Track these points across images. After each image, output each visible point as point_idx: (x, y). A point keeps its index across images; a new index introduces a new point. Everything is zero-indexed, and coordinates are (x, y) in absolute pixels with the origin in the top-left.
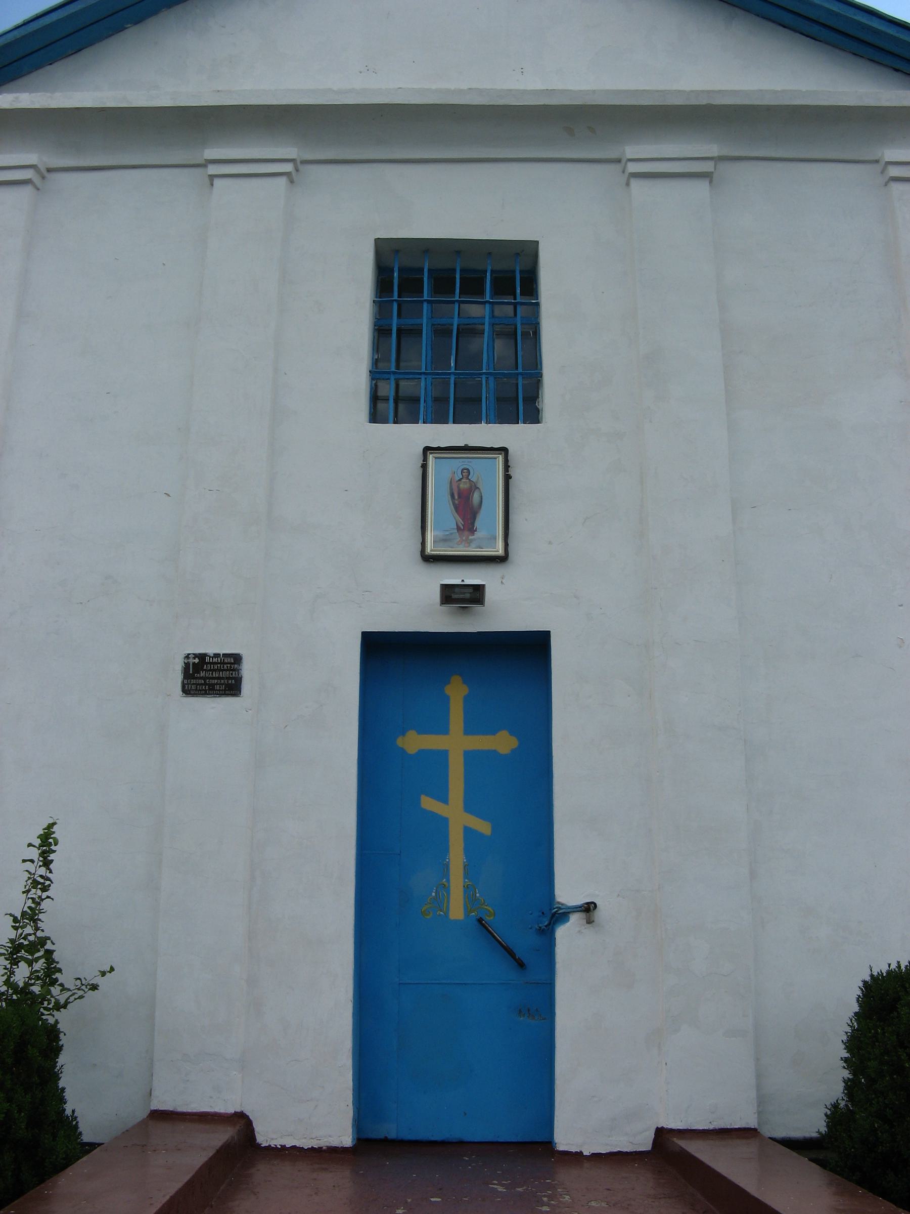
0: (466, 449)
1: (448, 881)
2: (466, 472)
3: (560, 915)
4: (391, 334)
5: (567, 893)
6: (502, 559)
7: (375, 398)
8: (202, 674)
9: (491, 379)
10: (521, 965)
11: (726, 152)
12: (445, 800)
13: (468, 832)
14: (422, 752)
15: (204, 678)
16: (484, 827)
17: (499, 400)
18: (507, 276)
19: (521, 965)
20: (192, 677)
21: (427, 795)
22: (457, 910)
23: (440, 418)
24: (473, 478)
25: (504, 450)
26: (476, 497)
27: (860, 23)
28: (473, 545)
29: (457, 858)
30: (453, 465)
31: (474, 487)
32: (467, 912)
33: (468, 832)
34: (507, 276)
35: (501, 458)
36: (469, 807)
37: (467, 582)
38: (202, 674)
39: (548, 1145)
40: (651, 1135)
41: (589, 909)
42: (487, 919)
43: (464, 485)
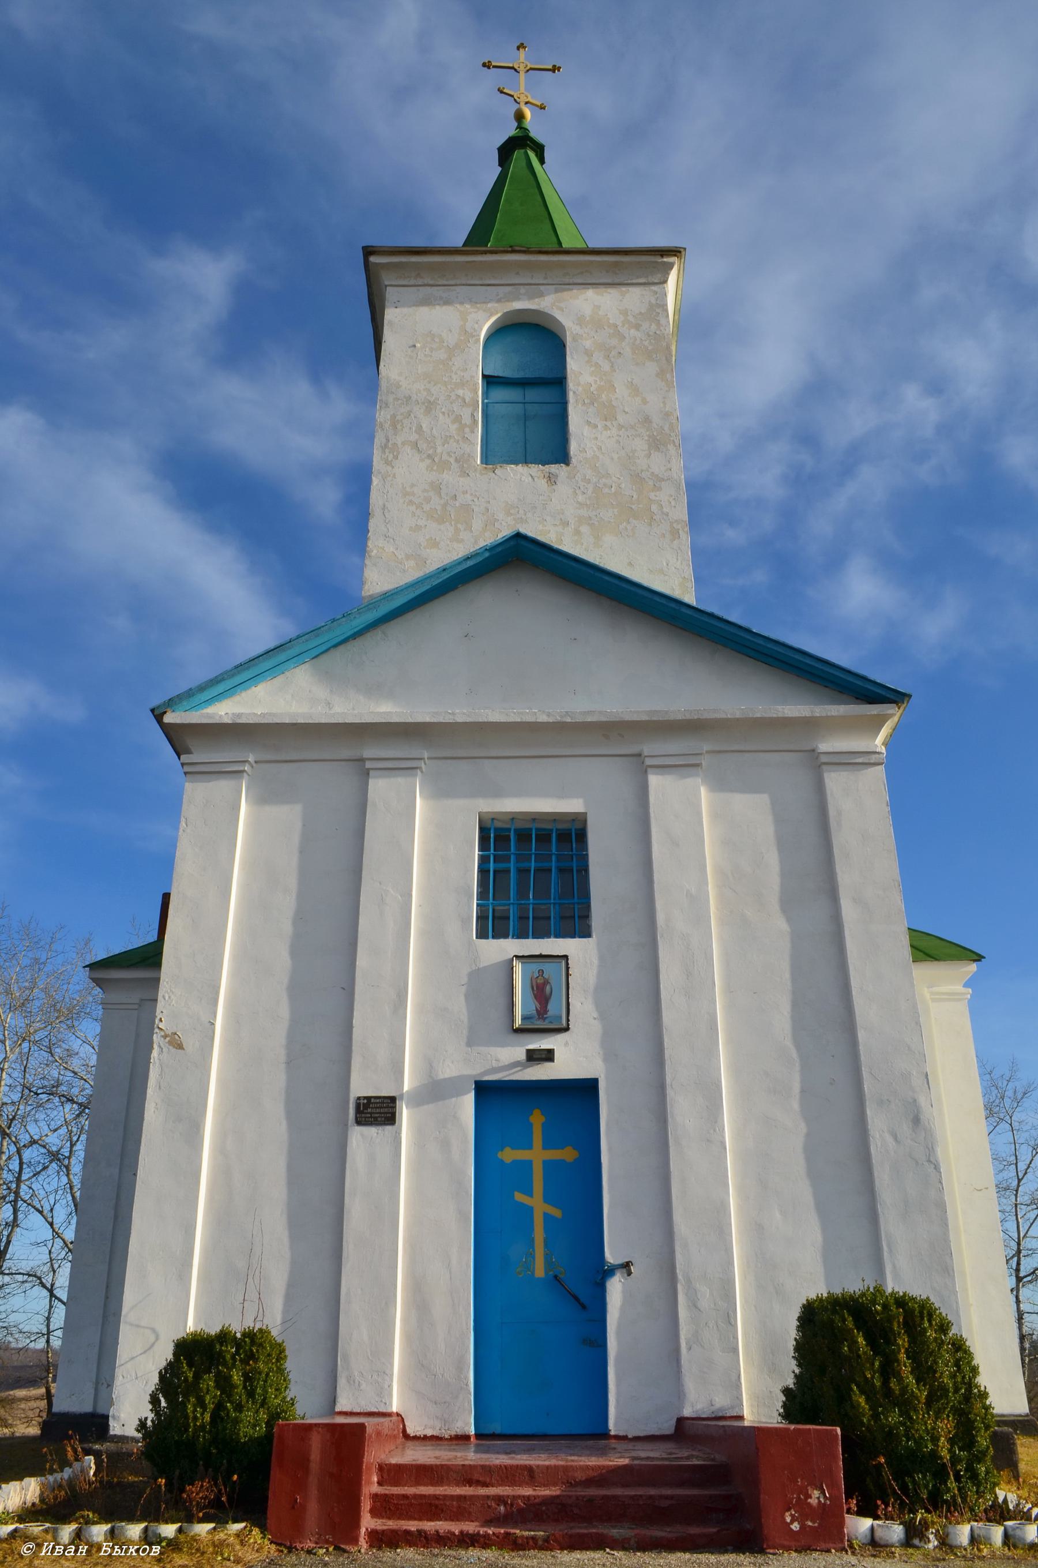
0: (541, 956)
1: (534, 1250)
2: (541, 972)
3: (609, 1272)
4: (491, 880)
5: (611, 1256)
6: (567, 1029)
7: (482, 918)
8: (369, 1110)
9: (557, 907)
10: (584, 1307)
11: (717, 748)
12: (545, 1214)
13: (530, 1193)
14: (531, 1125)
15: (371, 1113)
16: (557, 1213)
17: (563, 918)
18: (567, 837)
19: (584, 1307)
20: (363, 1112)
21: (361, 589)
22: (540, 1271)
23: (522, 934)
24: (546, 975)
25: (566, 957)
26: (548, 988)
27: (806, 664)
28: (547, 1021)
29: (539, 1234)
30: (535, 967)
31: (546, 982)
32: (546, 1271)
33: (546, 1216)
34: (567, 837)
35: (563, 962)
36: (546, 1200)
37: (543, 1047)
38: (369, 1110)
39: (605, 1435)
40: (673, 1422)
41: (626, 1266)
42: (561, 1276)
43: (540, 981)
